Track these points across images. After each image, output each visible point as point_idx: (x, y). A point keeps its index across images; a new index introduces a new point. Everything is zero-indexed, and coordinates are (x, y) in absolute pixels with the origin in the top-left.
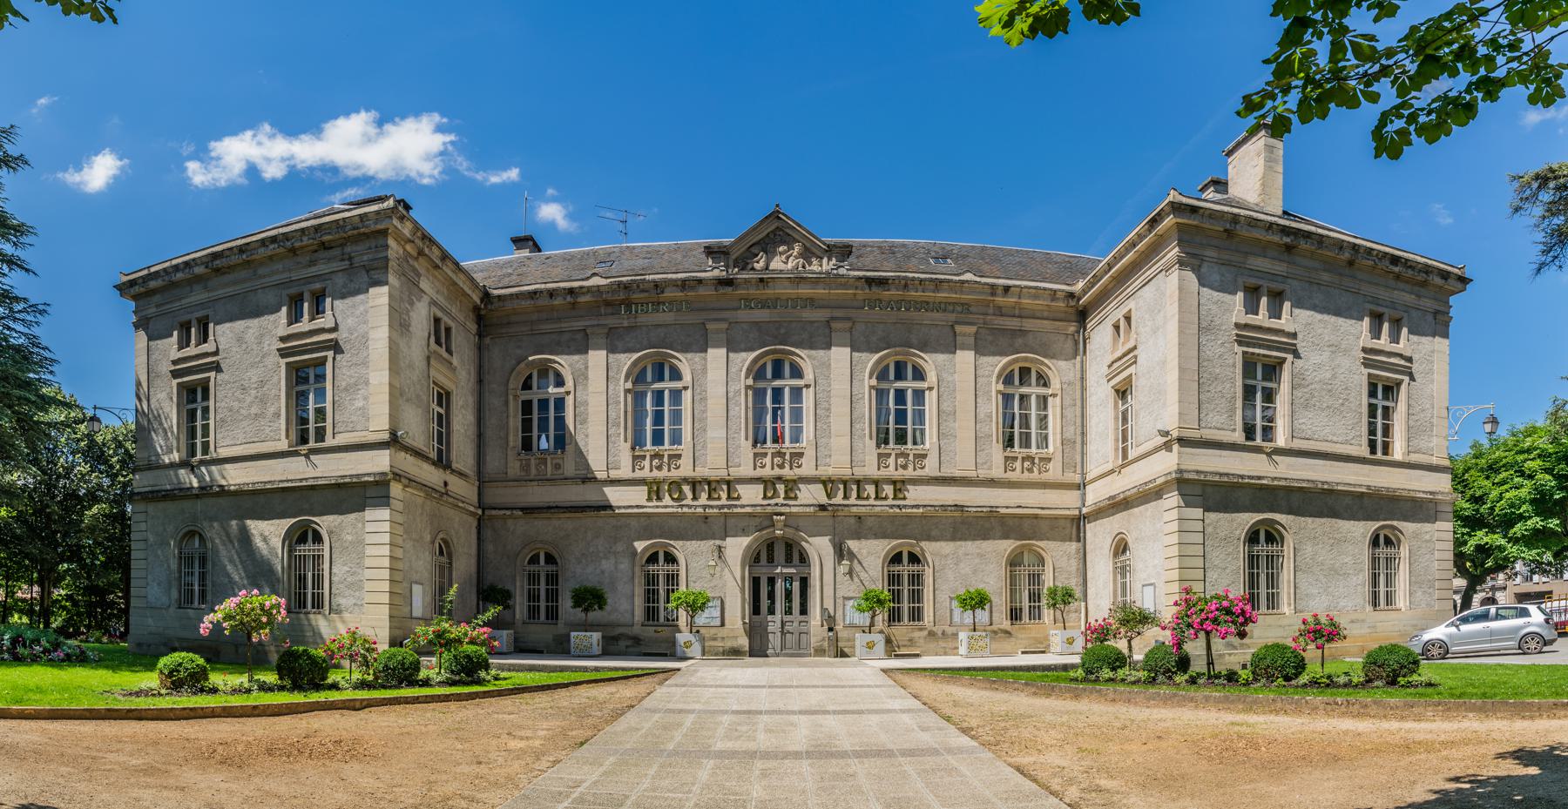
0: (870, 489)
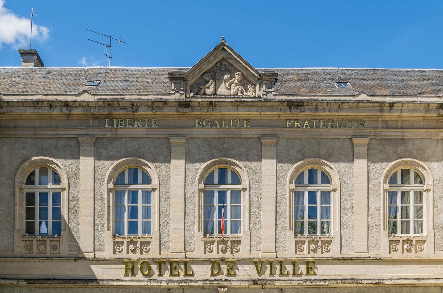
0: (290, 268)
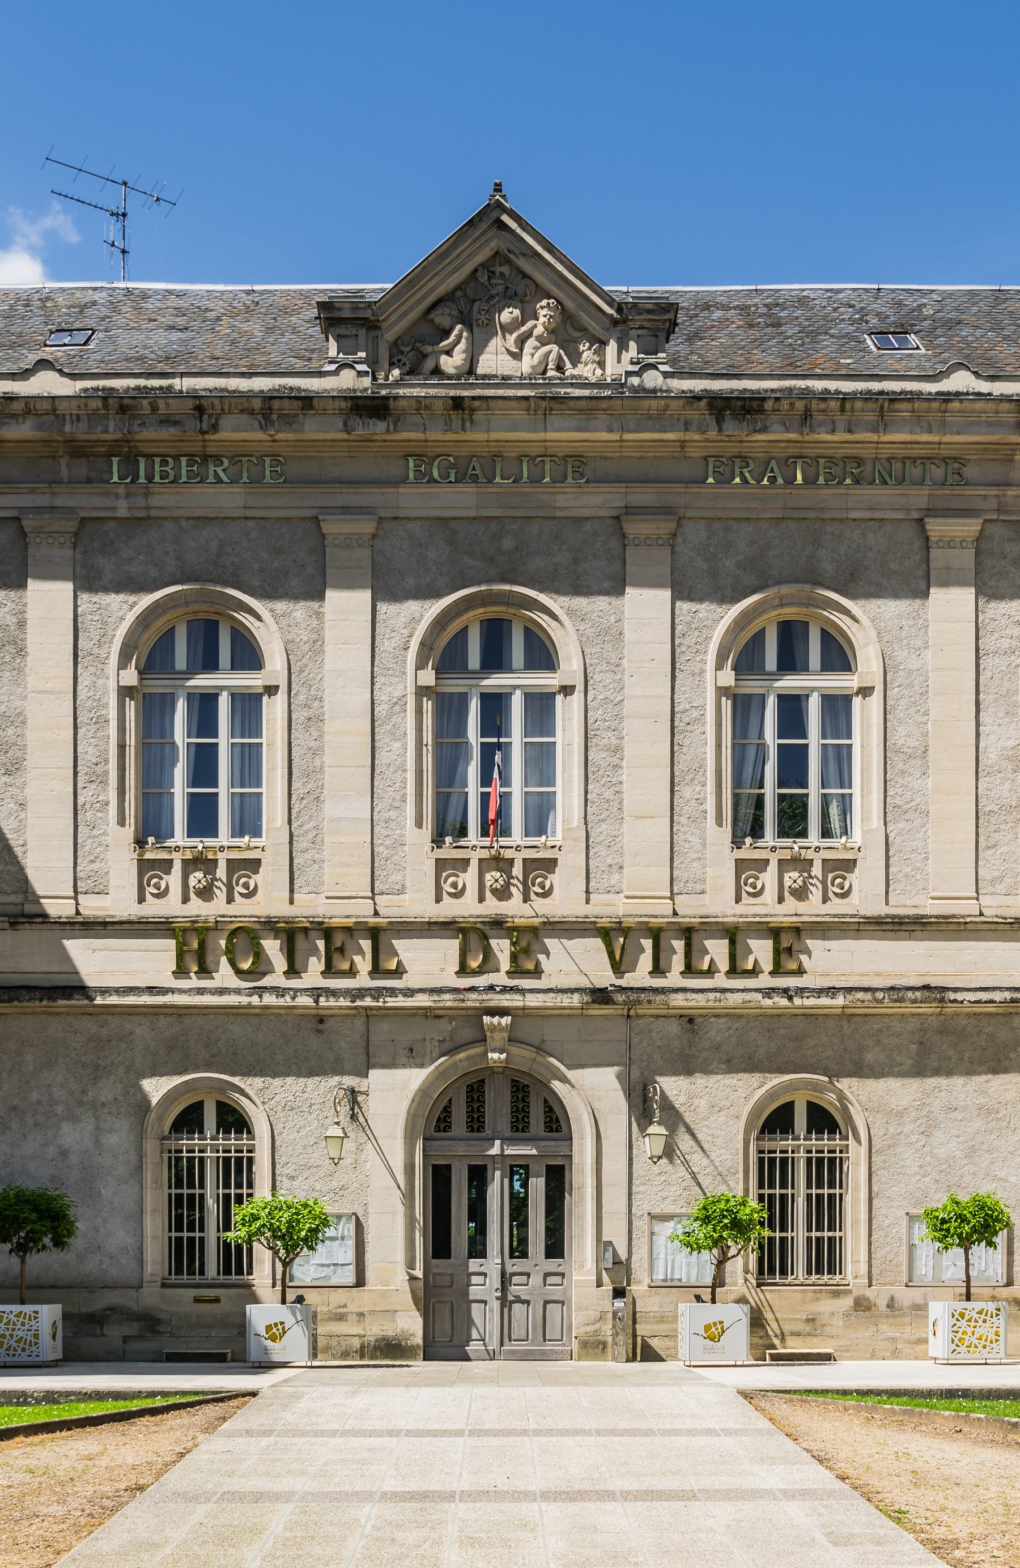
0: (717, 950)
